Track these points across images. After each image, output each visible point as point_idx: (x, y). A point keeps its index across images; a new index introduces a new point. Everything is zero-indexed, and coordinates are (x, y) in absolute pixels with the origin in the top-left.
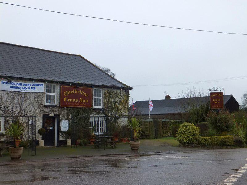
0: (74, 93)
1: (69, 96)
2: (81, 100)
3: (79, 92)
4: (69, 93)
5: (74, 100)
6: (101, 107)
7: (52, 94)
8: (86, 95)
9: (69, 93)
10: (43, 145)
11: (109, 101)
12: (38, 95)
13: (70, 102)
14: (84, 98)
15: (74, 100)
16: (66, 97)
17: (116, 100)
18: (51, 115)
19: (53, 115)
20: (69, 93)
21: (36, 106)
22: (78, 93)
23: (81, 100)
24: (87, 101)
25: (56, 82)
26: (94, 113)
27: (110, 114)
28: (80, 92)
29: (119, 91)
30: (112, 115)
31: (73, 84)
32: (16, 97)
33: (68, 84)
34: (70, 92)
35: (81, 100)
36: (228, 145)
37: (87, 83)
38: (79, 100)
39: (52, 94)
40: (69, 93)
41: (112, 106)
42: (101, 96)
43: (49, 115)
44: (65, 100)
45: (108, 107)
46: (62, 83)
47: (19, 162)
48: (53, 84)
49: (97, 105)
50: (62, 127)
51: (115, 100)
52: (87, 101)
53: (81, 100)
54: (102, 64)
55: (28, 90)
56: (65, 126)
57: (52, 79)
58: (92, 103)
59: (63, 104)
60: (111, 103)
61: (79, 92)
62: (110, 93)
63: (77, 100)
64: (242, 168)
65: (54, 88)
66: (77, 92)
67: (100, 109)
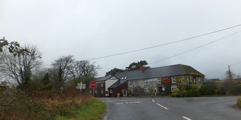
1: (164, 81)
11: (178, 80)
12: (156, 82)
14: (168, 80)
17: (181, 80)
21: (156, 84)
24: (169, 81)
26: (172, 85)
27: (179, 85)
29: (182, 76)
30: (179, 85)
36: (174, 97)
41: (179, 82)
45: (178, 82)
47: (234, 95)
51: (180, 79)
52: (169, 81)
54: (184, 65)
55: (153, 81)
56: (163, 89)
57: (146, 78)
59: (162, 83)
60: (179, 81)
62: (178, 77)
67: (175, 83)
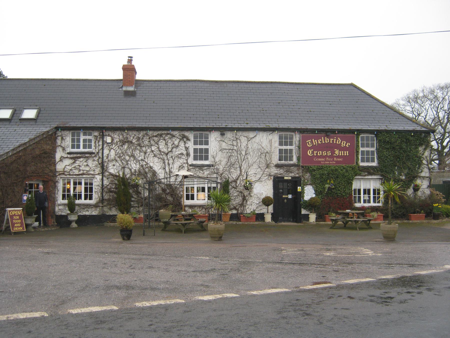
0: (323, 142)
1: (314, 148)
2: (336, 152)
3: (333, 141)
4: (315, 142)
5: (325, 153)
6: (375, 164)
7: (289, 147)
8: (346, 144)
9: (315, 142)
10: (270, 221)
13: (317, 156)
15: (325, 153)
16: (310, 148)
18: (285, 178)
19: (290, 178)
20: (315, 142)
22: (331, 142)
23: (337, 152)
24: (347, 153)
25: (294, 130)
28: (335, 140)
31: (321, 131)
32: (233, 155)
33: (313, 131)
34: (316, 141)
35: (337, 152)
37: (347, 127)
38: (333, 152)
39: (289, 147)
40: (315, 142)
42: (374, 161)
43: (284, 177)
44: (309, 153)
46: (301, 131)
48: (289, 133)
49: (368, 161)
50: (305, 195)
52: (347, 153)
53: (336, 152)
58: (358, 158)
61: (333, 141)
63: (329, 153)
64: (355, 177)
65: (292, 138)
66: (330, 141)
